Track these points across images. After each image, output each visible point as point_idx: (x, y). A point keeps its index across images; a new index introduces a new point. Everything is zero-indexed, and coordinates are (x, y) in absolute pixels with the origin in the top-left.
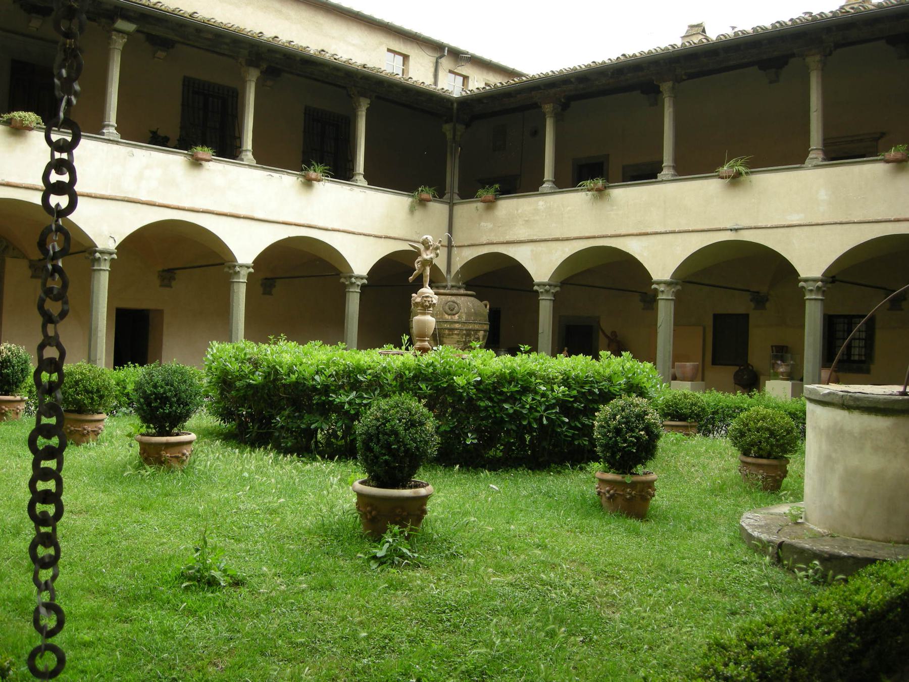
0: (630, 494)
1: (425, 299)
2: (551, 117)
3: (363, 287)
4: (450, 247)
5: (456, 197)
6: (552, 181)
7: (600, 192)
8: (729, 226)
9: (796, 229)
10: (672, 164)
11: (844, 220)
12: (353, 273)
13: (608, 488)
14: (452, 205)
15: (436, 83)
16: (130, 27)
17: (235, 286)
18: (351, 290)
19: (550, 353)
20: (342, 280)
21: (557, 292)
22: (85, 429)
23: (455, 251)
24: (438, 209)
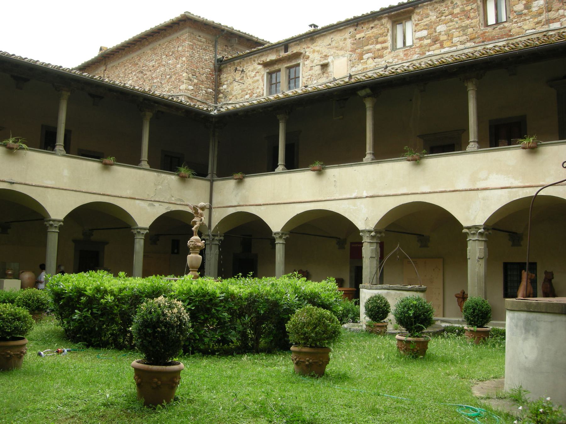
0: (308, 361)
2: (282, 122)
3: (60, 228)
5: (215, 176)
6: (283, 165)
8: (6, 179)
9: (50, 189)
10: (372, 152)
11: (77, 190)
13: (308, 359)
21: (287, 237)
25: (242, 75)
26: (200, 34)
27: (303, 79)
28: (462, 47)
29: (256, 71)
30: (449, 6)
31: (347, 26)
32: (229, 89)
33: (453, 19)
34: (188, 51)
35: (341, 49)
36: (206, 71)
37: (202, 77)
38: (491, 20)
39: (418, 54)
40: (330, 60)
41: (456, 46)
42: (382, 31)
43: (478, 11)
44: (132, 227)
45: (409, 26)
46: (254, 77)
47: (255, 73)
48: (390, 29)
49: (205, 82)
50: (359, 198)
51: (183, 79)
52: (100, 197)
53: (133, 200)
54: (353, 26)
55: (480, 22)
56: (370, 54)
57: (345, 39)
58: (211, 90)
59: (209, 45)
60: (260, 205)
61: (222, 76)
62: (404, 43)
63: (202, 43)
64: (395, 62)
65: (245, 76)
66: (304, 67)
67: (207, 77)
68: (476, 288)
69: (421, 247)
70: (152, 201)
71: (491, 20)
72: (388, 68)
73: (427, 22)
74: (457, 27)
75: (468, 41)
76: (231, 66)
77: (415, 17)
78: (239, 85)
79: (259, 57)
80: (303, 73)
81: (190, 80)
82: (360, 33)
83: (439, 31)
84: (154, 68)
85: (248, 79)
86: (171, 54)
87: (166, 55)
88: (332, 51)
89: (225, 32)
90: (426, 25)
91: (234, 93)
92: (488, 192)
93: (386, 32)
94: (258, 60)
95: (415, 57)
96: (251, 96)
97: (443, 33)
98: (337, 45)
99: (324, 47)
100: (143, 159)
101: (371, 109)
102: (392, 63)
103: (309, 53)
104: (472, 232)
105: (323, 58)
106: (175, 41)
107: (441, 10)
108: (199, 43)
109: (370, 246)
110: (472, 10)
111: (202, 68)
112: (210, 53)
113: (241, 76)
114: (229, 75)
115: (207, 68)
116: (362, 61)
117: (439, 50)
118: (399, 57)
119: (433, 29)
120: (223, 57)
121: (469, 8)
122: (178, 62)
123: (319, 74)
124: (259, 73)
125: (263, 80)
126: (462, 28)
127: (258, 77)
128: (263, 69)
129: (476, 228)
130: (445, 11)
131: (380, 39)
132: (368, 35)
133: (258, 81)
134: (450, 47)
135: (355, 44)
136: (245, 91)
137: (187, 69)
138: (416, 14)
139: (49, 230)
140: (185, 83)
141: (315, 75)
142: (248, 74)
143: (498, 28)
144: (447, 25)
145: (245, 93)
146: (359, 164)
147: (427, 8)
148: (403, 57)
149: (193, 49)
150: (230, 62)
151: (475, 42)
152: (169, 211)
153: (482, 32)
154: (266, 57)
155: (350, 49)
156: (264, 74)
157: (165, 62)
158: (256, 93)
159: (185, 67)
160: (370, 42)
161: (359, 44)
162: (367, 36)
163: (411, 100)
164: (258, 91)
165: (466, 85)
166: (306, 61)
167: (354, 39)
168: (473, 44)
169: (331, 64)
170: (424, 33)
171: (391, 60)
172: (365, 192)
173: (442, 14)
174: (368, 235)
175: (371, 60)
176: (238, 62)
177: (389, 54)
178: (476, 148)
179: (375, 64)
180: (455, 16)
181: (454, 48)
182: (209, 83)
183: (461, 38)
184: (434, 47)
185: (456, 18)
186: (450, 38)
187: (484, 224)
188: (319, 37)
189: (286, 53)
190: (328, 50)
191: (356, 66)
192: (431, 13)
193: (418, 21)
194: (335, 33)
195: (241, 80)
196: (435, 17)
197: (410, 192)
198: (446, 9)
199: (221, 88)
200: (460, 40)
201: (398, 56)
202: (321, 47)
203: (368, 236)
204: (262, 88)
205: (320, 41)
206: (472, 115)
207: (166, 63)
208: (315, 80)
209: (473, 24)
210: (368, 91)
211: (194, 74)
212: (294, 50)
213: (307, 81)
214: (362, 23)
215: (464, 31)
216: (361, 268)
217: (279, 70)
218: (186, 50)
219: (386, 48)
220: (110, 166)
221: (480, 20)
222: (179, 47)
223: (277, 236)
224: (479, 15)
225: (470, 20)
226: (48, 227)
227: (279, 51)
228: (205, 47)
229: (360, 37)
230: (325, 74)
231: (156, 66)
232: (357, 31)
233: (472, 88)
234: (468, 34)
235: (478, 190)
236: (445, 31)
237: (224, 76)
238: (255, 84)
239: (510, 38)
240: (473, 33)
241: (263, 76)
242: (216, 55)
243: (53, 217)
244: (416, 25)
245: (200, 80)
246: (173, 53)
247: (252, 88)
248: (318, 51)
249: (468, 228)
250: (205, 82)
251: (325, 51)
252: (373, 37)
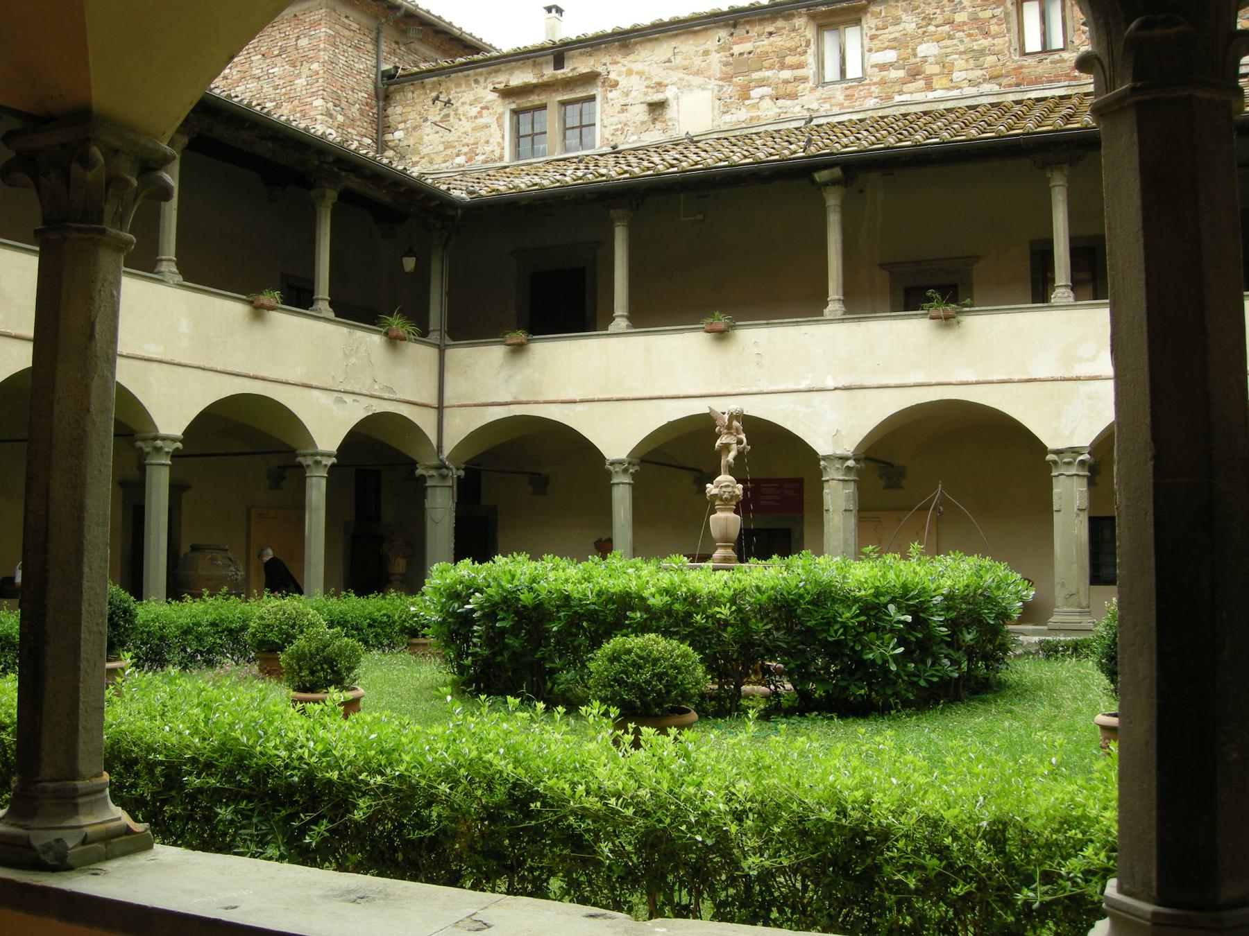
1: (724, 489)
3: (175, 455)
7: (722, 335)
9: (155, 365)
10: (626, 314)
11: (207, 366)
12: (316, 447)
14: (442, 350)
18: (153, 461)
20: (139, 444)
24: (421, 355)
25: (445, 111)
26: (349, 12)
27: (603, 129)
28: (973, 91)
29: (481, 105)
30: (944, 6)
31: (713, 25)
32: (411, 142)
33: (954, 34)
34: (325, 49)
35: (697, 73)
36: (360, 98)
37: (353, 110)
38: (1033, 42)
39: (876, 97)
40: (669, 93)
41: (960, 88)
42: (793, 43)
43: (1008, 23)
44: (298, 452)
45: (852, 37)
46: (476, 117)
47: (478, 109)
48: (812, 40)
49: (359, 123)
50: (816, 391)
51: (315, 113)
52: (248, 382)
53: (307, 391)
54: (726, 26)
55: (1010, 45)
56: (765, 88)
57: (706, 53)
58: (370, 141)
59: (365, 38)
60: (574, 402)
61: (390, 111)
62: (843, 72)
63: (351, 34)
64: (826, 110)
65: (452, 113)
66: (606, 105)
67: (361, 111)
68: (1075, 566)
69: (886, 488)
70: (340, 391)
71: (1033, 42)
72: (814, 120)
73: (897, 35)
74: (963, 50)
75: (985, 80)
76: (416, 90)
77: (869, 21)
78: (437, 132)
79: (490, 73)
80: (604, 117)
81: (331, 116)
82: (741, 43)
83: (922, 55)
84: (229, 81)
85: (460, 120)
86: (276, 53)
87: (263, 55)
88: (676, 76)
89: (403, 11)
90: (895, 39)
91: (424, 151)
93: (804, 45)
94: (485, 81)
95: (871, 103)
96: (470, 159)
97: (931, 60)
98: (686, 63)
99: (655, 65)
100: (320, 296)
101: (838, 209)
102: (817, 110)
103: (619, 75)
104: (1066, 460)
105: (652, 88)
106: (288, 24)
107: (927, 12)
108: (347, 33)
109: (844, 488)
110: (995, 20)
111: (353, 90)
112: (367, 58)
113: (443, 113)
114: (409, 109)
115: (361, 92)
116: (747, 102)
117: (924, 93)
118: (834, 101)
119: (910, 51)
120: (396, 68)
121: (988, 14)
122: (297, 72)
123: (643, 123)
124: (491, 111)
125: (501, 126)
126: (972, 54)
127: (487, 118)
128: (500, 101)
129: (1073, 452)
130: (935, 16)
131: (790, 60)
132: (761, 49)
133: (487, 127)
134: (948, 89)
135: (731, 64)
136: (454, 147)
137: (324, 90)
138: (872, 16)
139: (147, 462)
140: (319, 122)
141: (634, 123)
142: (461, 111)
143: (1048, 61)
144: (941, 44)
145: (455, 151)
146: (813, 321)
147: (897, 6)
148: (843, 101)
149: (334, 45)
150: (414, 80)
151: (1000, 85)
152: (370, 413)
153: (1014, 65)
154: (507, 76)
155: (719, 76)
156: (503, 113)
157: (260, 71)
158: (483, 154)
159: (318, 84)
160: (766, 64)
161: (738, 67)
162: (758, 51)
163: (861, 191)
164: (488, 149)
165: (1049, 175)
166: (611, 91)
167: (727, 54)
168: (996, 88)
169: (673, 103)
170: (891, 56)
171: (814, 106)
172: (829, 377)
173: (929, 20)
174: (838, 466)
175: (768, 101)
176: (434, 82)
177: (810, 92)
178: (1071, 299)
179: (778, 111)
180: (959, 27)
181: (956, 93)
182: (365, 124)
183: (970, 72)
184: (912, 86)
185: (959, 31)
186: (946, 71)
187: (1090, 445)
188: (641, 43)
189: (559, 72)
190: (665, 72)
191: (733, 110)
192: (904, 17)
193: (877, 30)
194: (682, 38)
195: (441, 121)
196: (913, 26)
197: (933, 382)
198: (938, 11)
199: (389, 137)
201: (830, 98)
202: (647, 63)
203: (838, 468)
204: (499, 144)
205: (646, 51)
206: (1062, 234)
207: (262, 72)
208: (633, 134)
209: (997, 48)
210: (837, 172)
211: (337, 102)
212: (578, 65)
213: (613, 135)
214: (748, 22)
215: (976, 59)
217: (543, 107)
218: (322, 46)
219: (804, 79)
220: (266, 312)
221: (1010, 41)
222: (298, 38)
223: (618, 468)
224: (1009, 31)
225: (990, 39)
226: (148, 453)
227: (541, 64)
228: (356, 42)
229: (741, 51)
230: (657, 123)
231: (235, 77)
232: (735, 38)
233: (1061, 183)
234: (986, 66)
235: (1078, 379)
236: (935, 56)
237: (395, 111)
238: (478, 134)
239: (1073, 83)
240: (996, 66)
241: (500, 117)
242: (378, 62)
243: (163, 430)
244: (872, 38)
245: (348, 118)
246: (283, 50)
247: (472, 142)
248: (640, 74)
249: (1058, 452)
250: (359, 123)
251: (658, 74)
252: (773, 54)
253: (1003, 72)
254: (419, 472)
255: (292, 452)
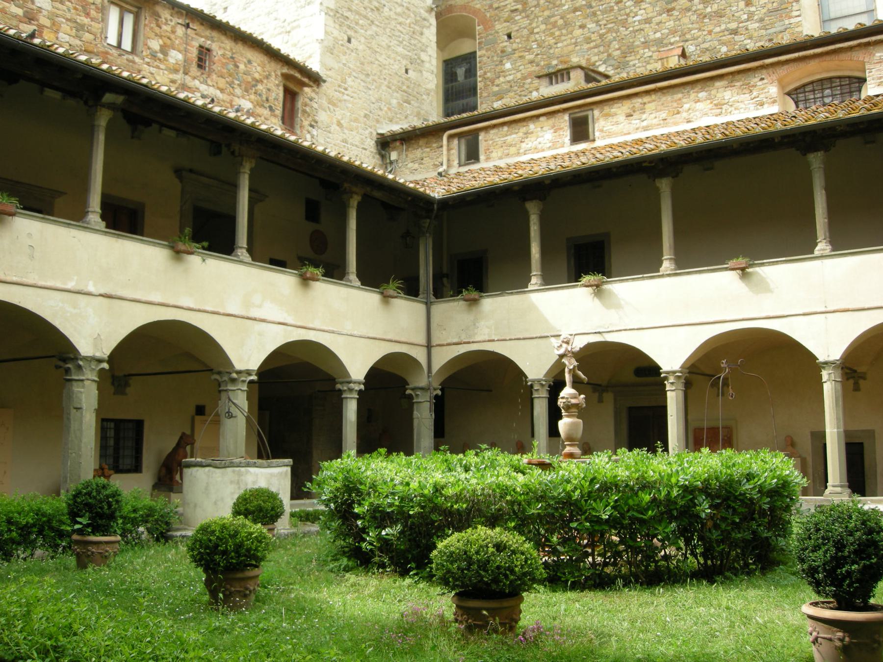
3: (360, 392)
4: (429, 347)
15: (289, 117)
16: (119, 99)
17: (76, 388)
19: (256, 455)
22: (89, 551)
23: (434, 351)
71: (112, 40)
92: (264, 324)
97: (45, 13)
183: (72, 39)
200: (71, 43)
215: (77, 30)
216: (825, 445)
234: (83, 39)
236: (48, 11)
243: (239, 366)
253: (95, 50)
254: (408, 392)
255: (332, 380)
